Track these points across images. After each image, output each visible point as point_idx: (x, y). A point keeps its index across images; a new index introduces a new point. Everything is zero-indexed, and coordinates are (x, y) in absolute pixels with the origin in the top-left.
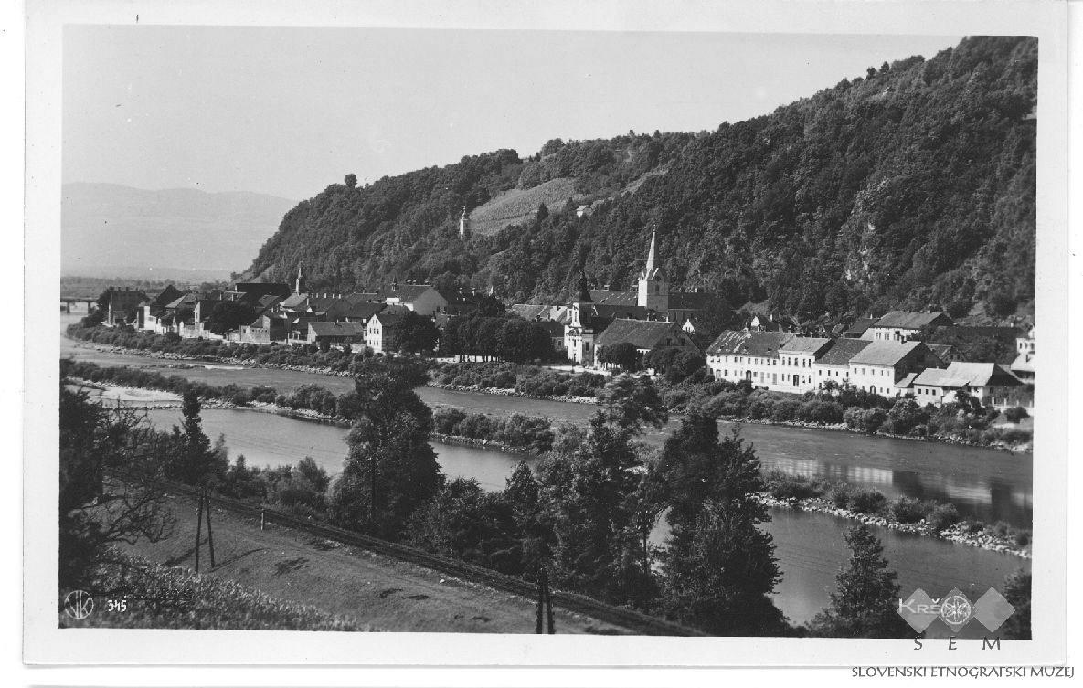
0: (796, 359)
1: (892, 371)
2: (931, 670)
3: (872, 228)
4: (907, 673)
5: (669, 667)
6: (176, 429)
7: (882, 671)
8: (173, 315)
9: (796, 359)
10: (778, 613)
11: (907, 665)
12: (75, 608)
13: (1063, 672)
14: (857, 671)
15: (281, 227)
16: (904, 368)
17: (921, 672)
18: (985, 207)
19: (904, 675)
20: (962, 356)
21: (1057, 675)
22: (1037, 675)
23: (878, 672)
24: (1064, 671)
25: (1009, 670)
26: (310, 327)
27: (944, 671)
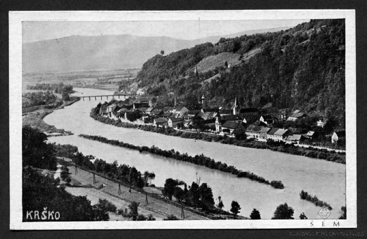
1: (282, 136)
3: (297, 83)
5: (116, 143)
6: (239, 212)
8: (119, 115)
10: (192, 184)
15: (165, 151)
16: (284, 136)
18: (324, 78)
26: (154, 120)
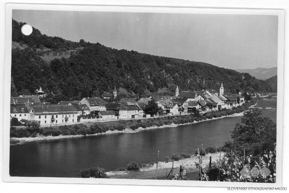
0: (63, 122)
2: (248, 189)
4: (242, 189)
7: (235, 189)
9: (63, 122)
11: (242, 187)
12: (242, 179)
13: (284, 189)
14: (229, 188)
17: (246, 189)
19: (241, 190)
20: (214, 68)
21: (282, 190)
22: (277, 189)
23: (234, 189)
24: (285, 189)
25: (228, 188)
27: (252, 189)
